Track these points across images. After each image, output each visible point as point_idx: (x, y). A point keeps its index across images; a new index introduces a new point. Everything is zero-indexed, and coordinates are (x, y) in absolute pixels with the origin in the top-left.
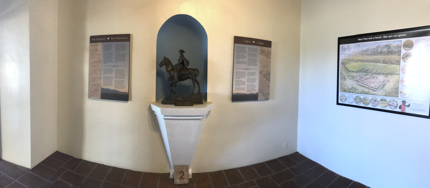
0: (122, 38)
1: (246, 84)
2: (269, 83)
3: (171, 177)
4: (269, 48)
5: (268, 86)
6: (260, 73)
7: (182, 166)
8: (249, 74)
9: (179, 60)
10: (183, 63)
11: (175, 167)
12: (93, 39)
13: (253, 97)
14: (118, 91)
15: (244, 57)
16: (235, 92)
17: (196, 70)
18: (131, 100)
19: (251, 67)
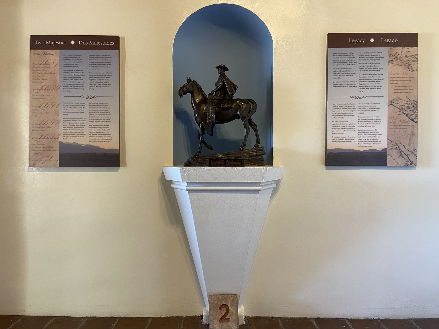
0: (102, 43)
1: (357, 127)
2: (414, 128)
3: (204, 321)
4: (412, 49)
5: (413, 134)
6: (391, 103)
7: (225, 296)
8: (364, 107)
9: (216, 85)
10: (225, 89)
11: (211, 296)
12: (38, 42)
13: (377, 159)
14: (97, 148)
15: (350, 73)
16: (332, 146)
17: (252, 101)
18: (125, 165)
19: (366, 92)
